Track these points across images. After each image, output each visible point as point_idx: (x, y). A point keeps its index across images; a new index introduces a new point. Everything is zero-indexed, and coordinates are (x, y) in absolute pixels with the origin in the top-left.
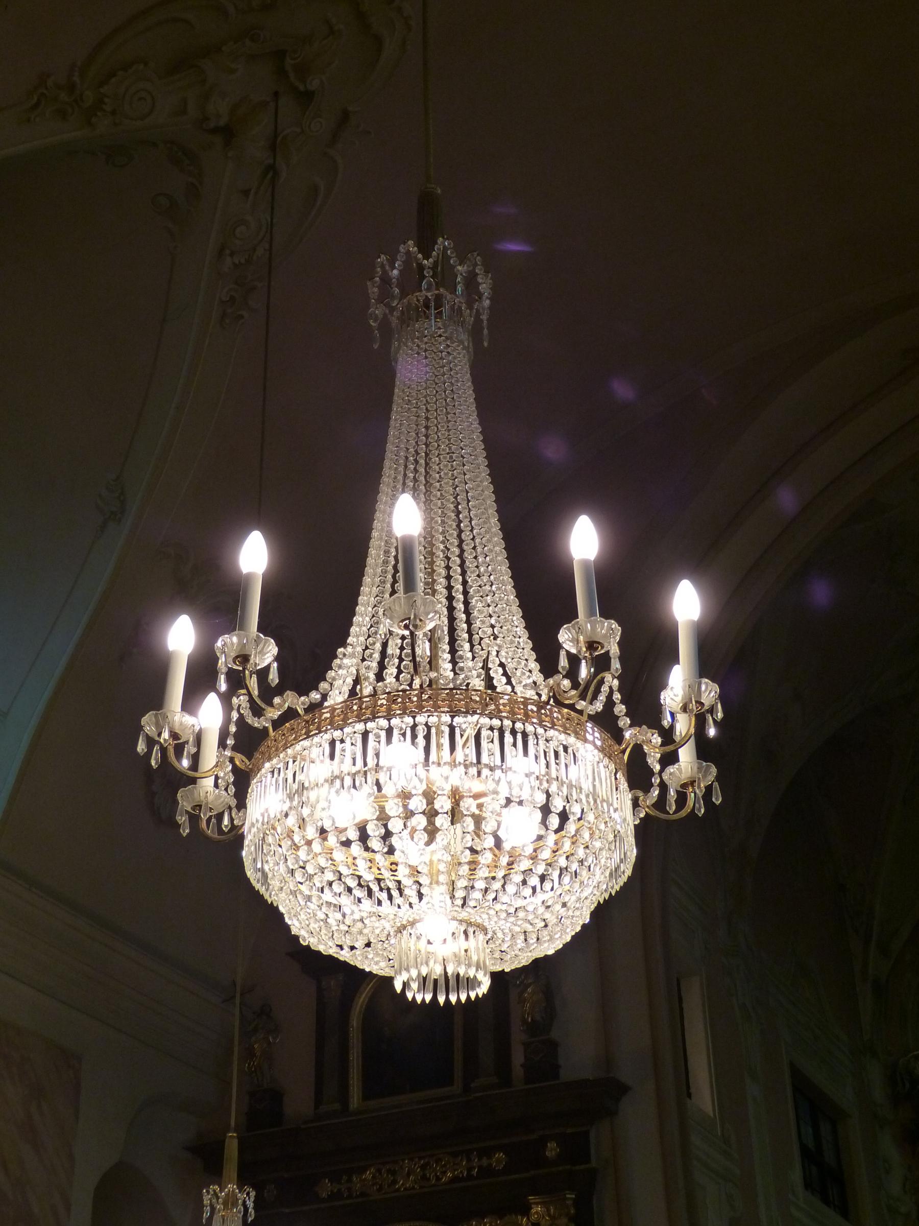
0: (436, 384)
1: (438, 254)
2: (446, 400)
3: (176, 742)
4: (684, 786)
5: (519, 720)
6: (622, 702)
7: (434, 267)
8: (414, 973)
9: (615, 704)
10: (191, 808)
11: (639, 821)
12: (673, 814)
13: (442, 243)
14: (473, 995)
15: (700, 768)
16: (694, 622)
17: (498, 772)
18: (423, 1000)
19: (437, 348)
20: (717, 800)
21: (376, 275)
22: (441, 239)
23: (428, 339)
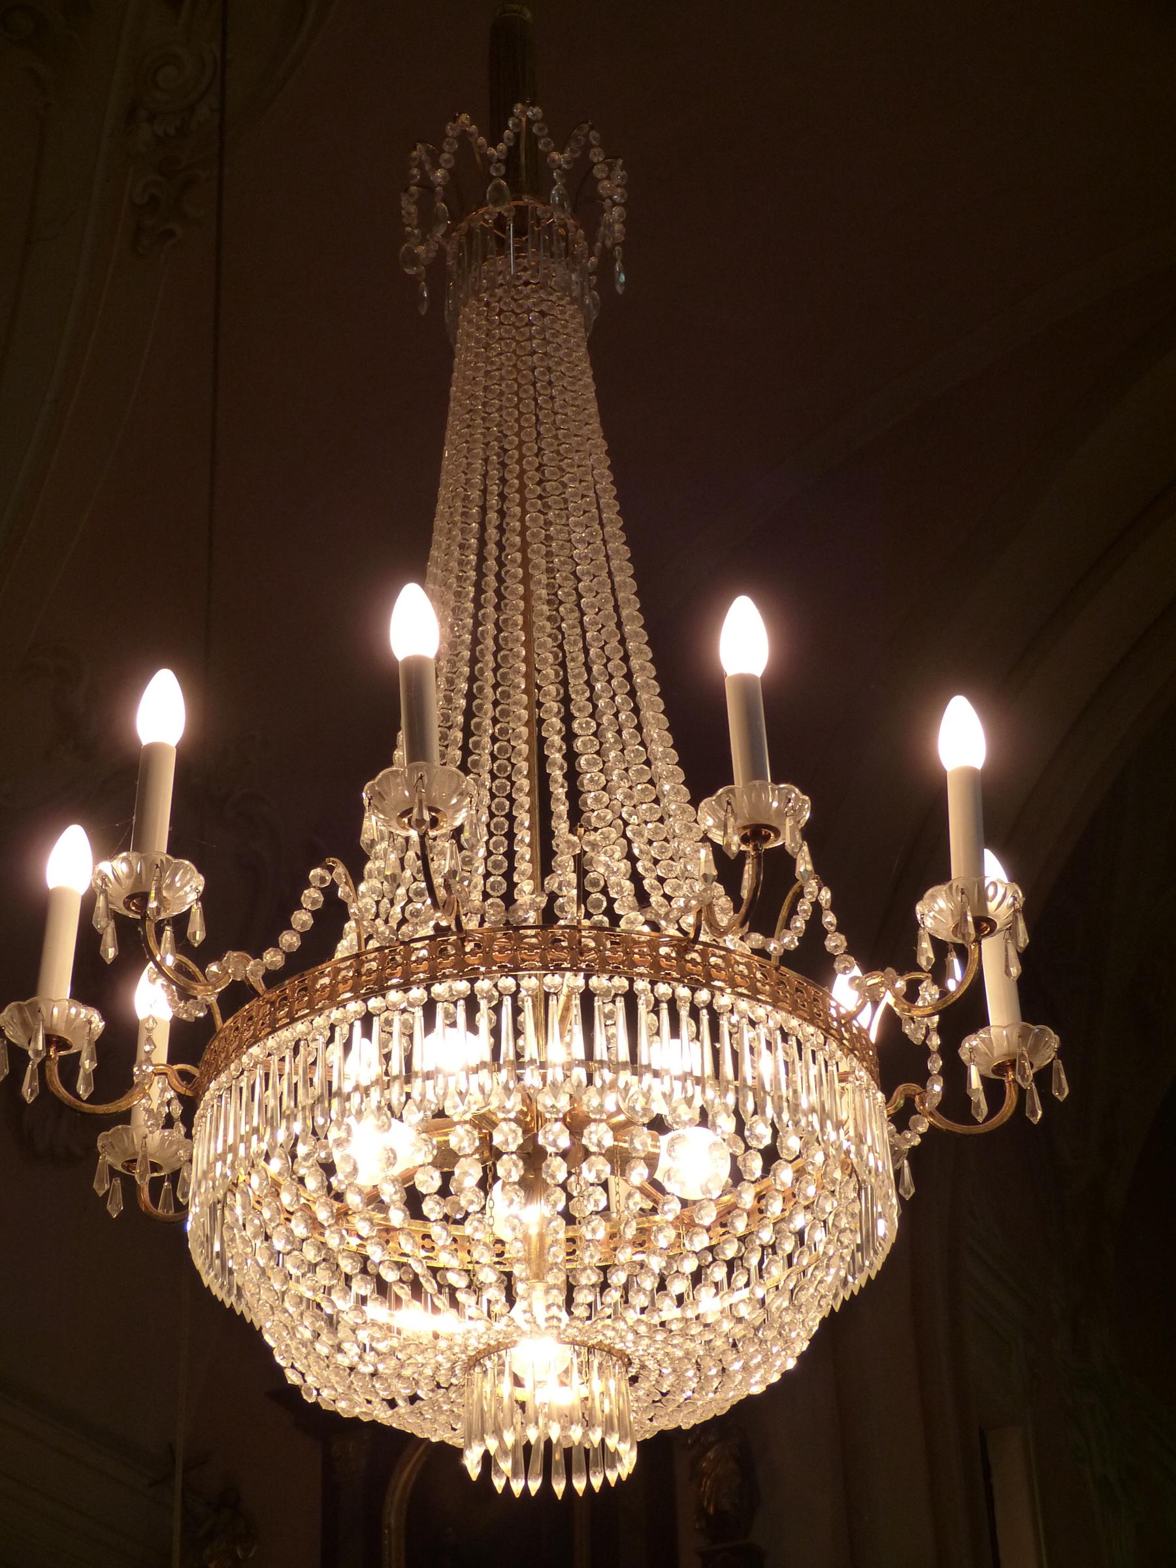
0: (519, 371)
1: (517, 136)
2: (535, 400)
3: (62, 1053)
4: (1000, 1069)
5: (641, 975)
6: (839, 929)
7: (511, 159)
8: (509, 1438)
9: (826, 932)
10: (123, 1166)
11: (919, 1140)
12: (984, 1121)
13: (525, 113)
14: (612, 1478)
15: (1023, 1036)
16: (973, 771)
17: (625, 1076)
18: (526, 1489)
19: (521, 306)
20: (1062, 1091)
21: (412, 182)
22: (519, 106)
23: (505, 291)
